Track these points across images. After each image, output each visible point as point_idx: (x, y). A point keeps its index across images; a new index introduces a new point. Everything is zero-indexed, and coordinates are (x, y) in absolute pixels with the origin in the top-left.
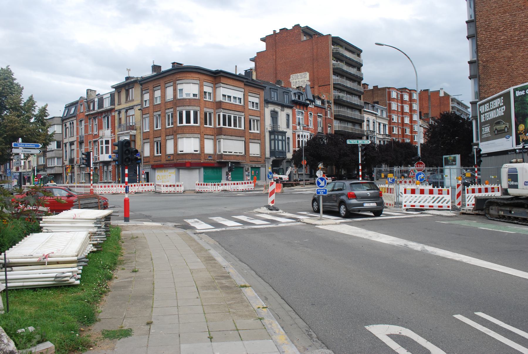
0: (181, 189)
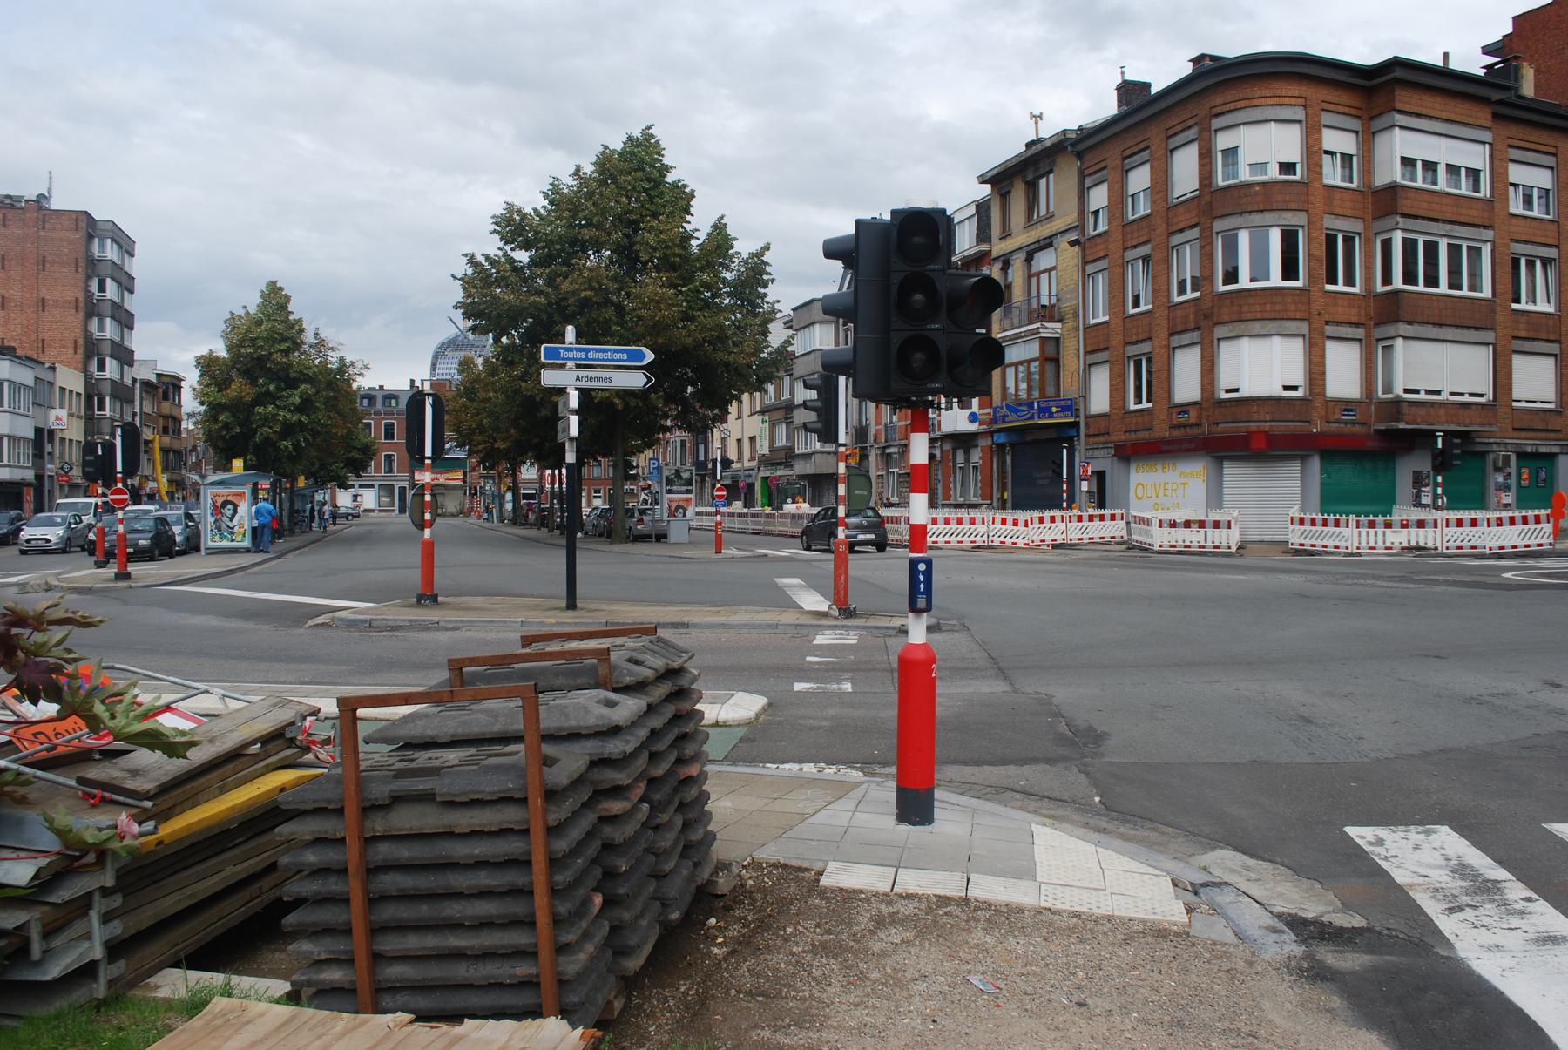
0: (1229, 539)
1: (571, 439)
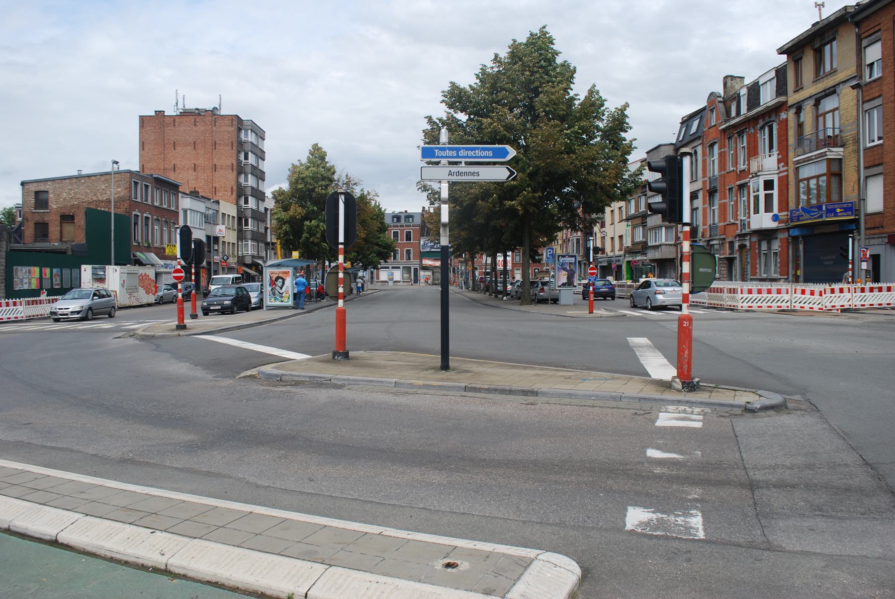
1: (445, 225)
